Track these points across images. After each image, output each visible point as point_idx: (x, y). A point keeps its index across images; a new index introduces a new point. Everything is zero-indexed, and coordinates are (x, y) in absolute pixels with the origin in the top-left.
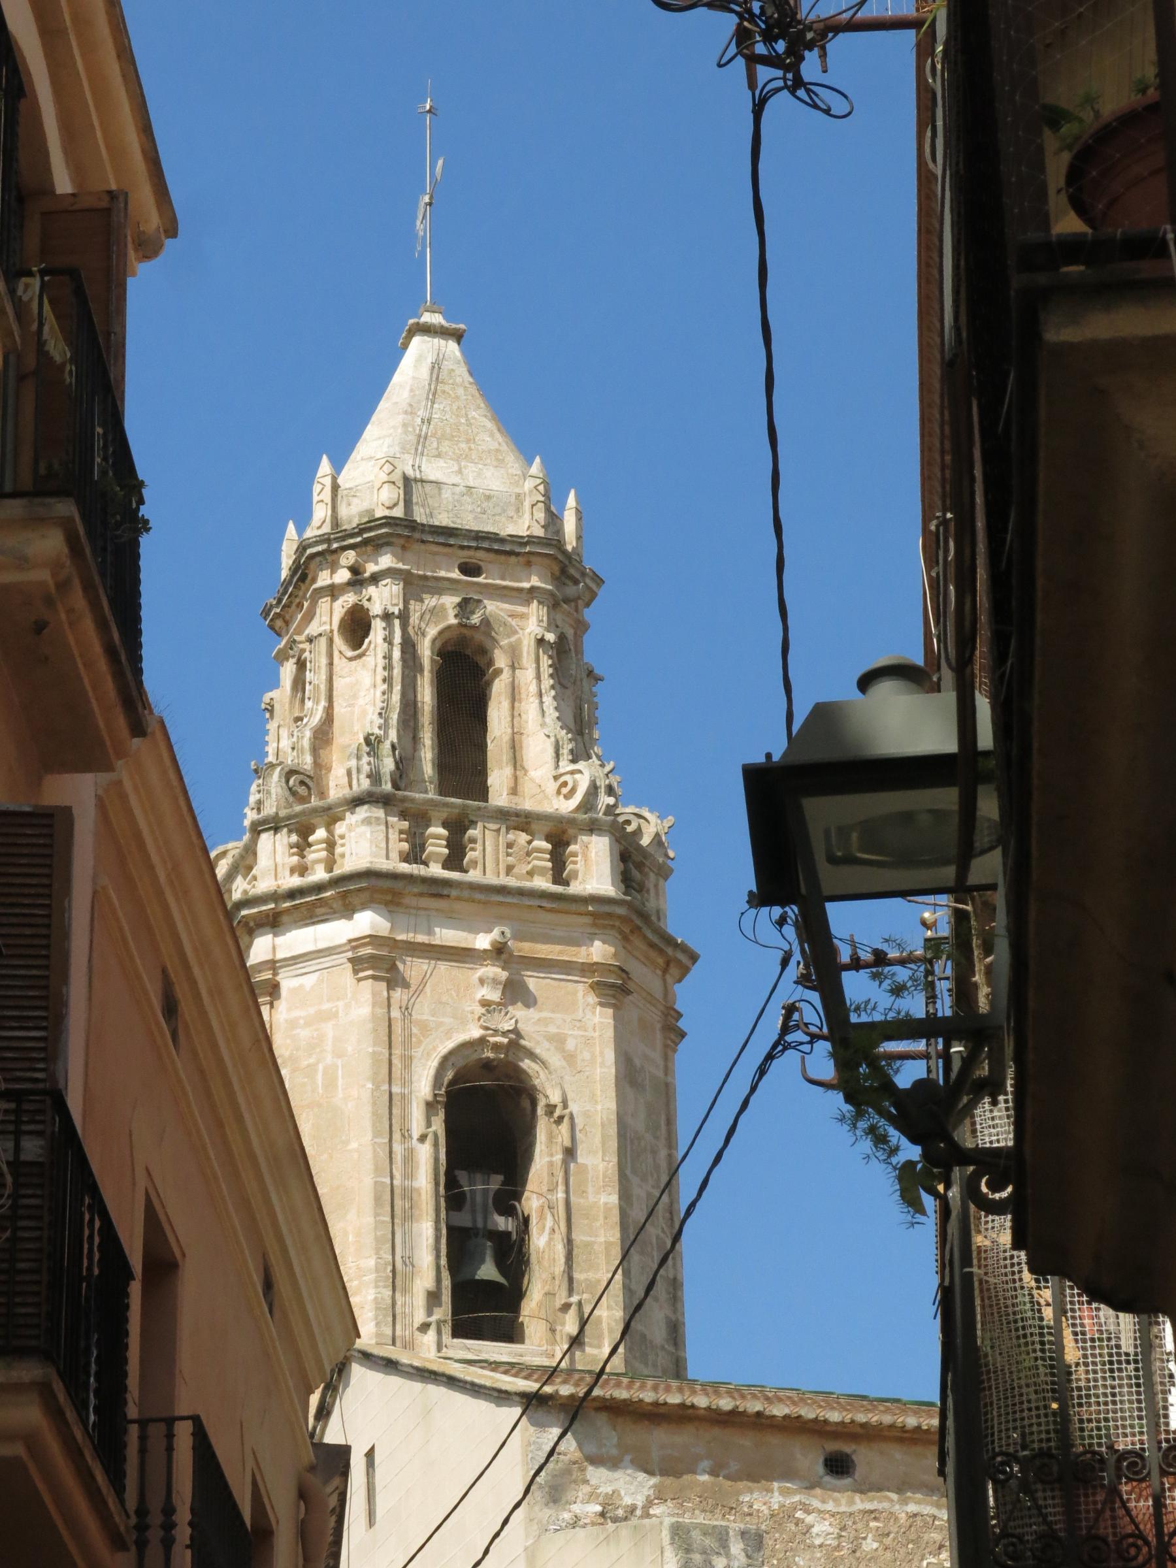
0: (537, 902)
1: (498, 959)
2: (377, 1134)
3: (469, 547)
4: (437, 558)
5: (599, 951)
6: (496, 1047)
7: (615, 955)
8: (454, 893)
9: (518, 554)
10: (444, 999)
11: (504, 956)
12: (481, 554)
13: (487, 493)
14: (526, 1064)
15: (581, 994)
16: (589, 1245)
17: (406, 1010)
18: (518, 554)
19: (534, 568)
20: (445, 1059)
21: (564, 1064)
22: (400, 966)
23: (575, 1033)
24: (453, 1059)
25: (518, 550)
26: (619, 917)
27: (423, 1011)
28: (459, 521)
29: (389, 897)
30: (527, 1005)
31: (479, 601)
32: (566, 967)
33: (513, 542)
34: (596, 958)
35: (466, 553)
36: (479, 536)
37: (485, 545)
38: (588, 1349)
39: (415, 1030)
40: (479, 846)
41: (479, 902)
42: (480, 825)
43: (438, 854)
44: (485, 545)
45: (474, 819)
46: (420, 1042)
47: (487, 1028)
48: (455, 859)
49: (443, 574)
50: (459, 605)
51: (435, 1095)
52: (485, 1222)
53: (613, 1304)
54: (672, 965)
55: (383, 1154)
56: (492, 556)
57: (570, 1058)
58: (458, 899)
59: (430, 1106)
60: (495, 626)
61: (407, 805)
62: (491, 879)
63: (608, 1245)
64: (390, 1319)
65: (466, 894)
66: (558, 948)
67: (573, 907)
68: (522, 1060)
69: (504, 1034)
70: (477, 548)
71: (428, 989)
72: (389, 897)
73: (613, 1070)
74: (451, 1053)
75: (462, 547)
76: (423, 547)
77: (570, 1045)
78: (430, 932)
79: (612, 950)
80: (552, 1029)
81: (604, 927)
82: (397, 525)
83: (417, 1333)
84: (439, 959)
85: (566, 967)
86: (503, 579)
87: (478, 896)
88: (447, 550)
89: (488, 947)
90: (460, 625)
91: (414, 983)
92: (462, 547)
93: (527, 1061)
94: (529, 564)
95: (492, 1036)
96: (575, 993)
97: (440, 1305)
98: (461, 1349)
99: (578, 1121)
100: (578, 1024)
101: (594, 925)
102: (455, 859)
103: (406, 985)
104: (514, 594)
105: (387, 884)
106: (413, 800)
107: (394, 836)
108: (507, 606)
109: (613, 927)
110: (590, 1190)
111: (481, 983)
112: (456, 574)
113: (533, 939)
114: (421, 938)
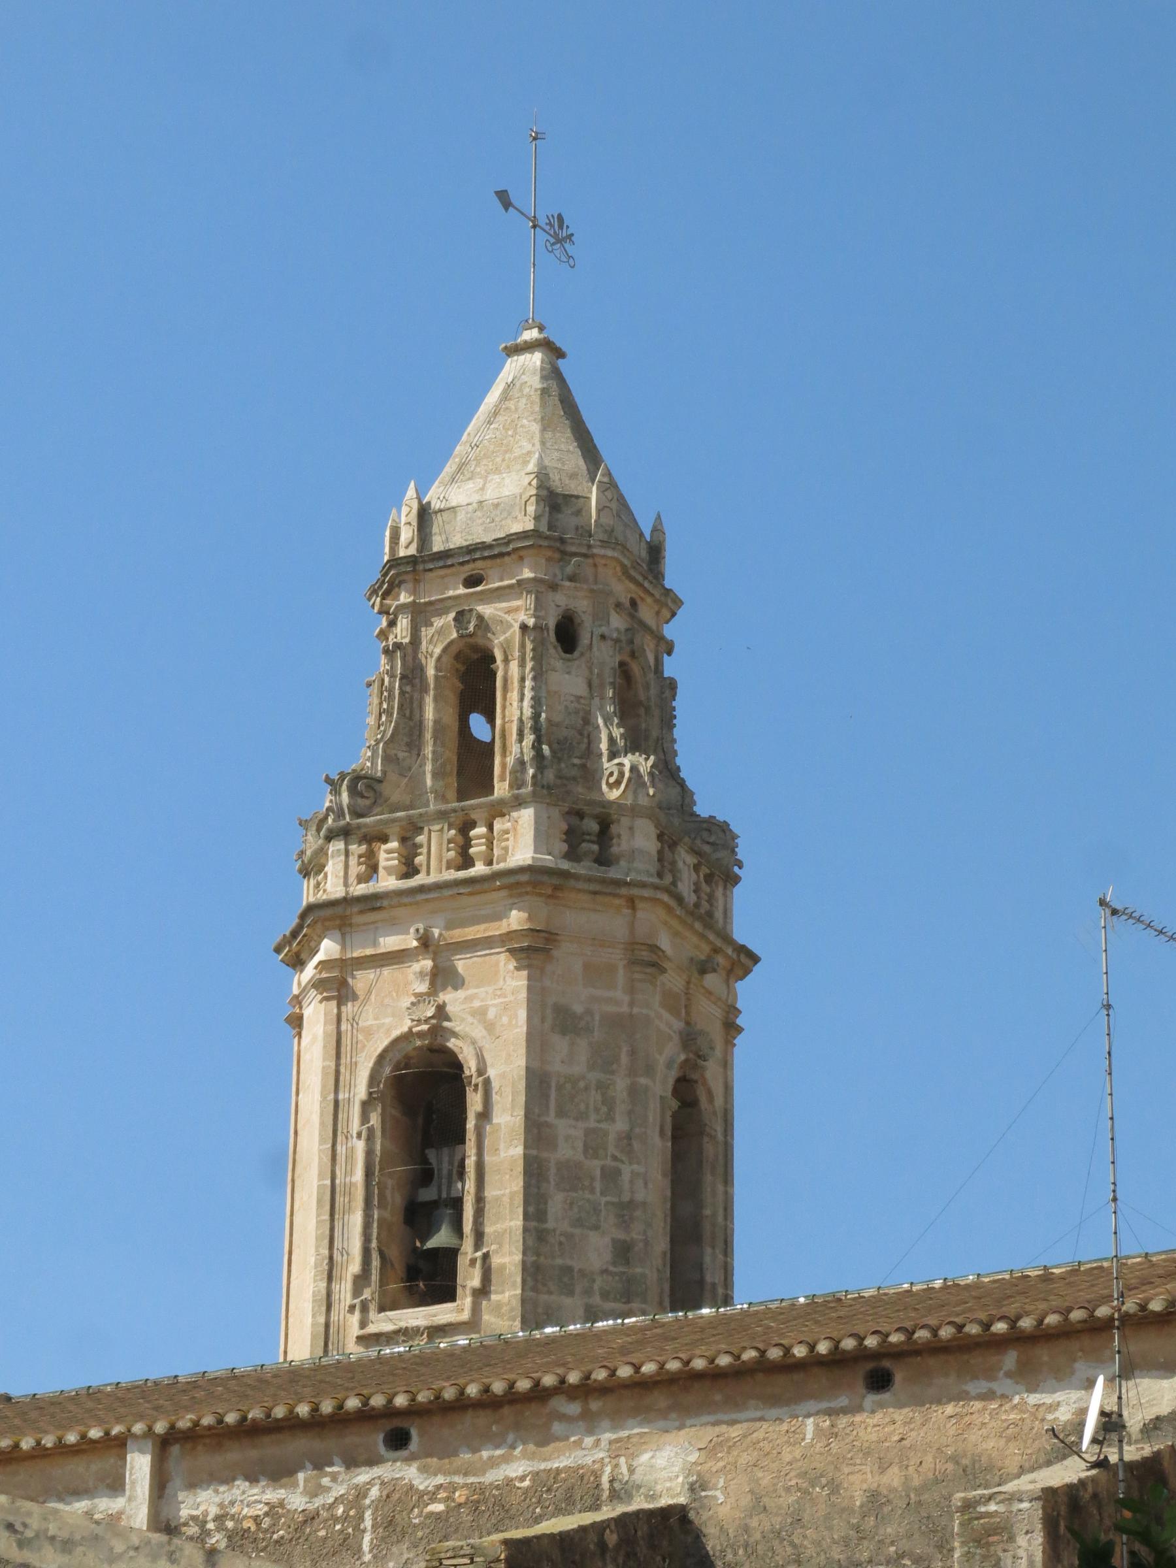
0: (456, 890)
1: (427, 952)
2: (322, 1141)
3: (468, 562)
4: (446, 580)
5: (516, 919)
6: (420, 1035)
7: (530, 919)
8: (385, 903)
9: (508, 554)
10: (386, 1001)
11: (431, 949)
12: (479, 564)
13: (496, 501)
14: (452, 1044)
15: (504, 963)
16: (497, 1199)
17: (354, 1021)
18: (508, 554)
19: (526, 561)
20: (381, 1057)
21: (484, 1032)
22: (350, 980)
23: (495, 1002)
24: (390, 1055)
25: (504, 550)
26: (528, 883)
27: (368, 1019)
28: (470, 538)
29: (338, 922)
30: (456, 988)
31: (471, 610)
32: (487, 943)
33: (499, 545)
34: (515, 926)
35: (467, 567)
36: (471, 549)
37: (477, 555)
38: (493, 1297)
39: (360, 1037)
40: (424, 850)
41: (411, 904)
42: (426, 829)
43: (480, 852)
44: (477, 555)
45: (421, 825)
46: (364, 1046)
47: (413, 1020)
48: (410, 870)
49: (451, 593)
50: (455, 619)
51: (370, 1094)
52: (449, 1192)
53: (514, 1250)
54: (637, 902)
55: (327, 1160)
56: (489, 563)
57: (490, 1027)
58: (392, 907)
59: (366, 1106)
60: (493, 627)
61: (363, 830)
62: (433, 878)
63: (512, 1196)
64: (324, 1308)
65: (395, 901)
66: (483, 926)
67: (486, 886)
68: (448, 1040)
69: (426, 1021)
70: (474, 560)
71: (373, 997)
72: (338, 922)
73: (525, 1029)
74: (385, 1051)
75: (462, 564)
76: (430, 574)
77: (491, 1014)
78: (375, 944)
79: (526, 915)
80: (477, 1004)
81: (520, 895)
82: (399, 565)
83: (348, 1315)
84: (383, 966)
85: (487, 943)
86: (502, 580)
87: (406, 900)
88: (453, 570)
89: (415, 943)
90: (461, 636)
91: (361, 993)
92: (462, 564)
93: (453, 1040)
94: (521, 558)
95: (417, 1026)
96: (497, 964)
97: (369, 1285)
98: (384, 1321)
99: (495, 1085)
100: (499, 993)
101: (511, 896)
102: (410, 870)
103: (355, 997)
104: (507, 591)
105: (328, 912)
106: (366, 825)
107: (353, 861)
108: (504, 605)
109: (527, 893)
110: (502, 1146)
111: (414, 976)
112: (462, 591)
113: (463, 924)
114: (369, 951)
